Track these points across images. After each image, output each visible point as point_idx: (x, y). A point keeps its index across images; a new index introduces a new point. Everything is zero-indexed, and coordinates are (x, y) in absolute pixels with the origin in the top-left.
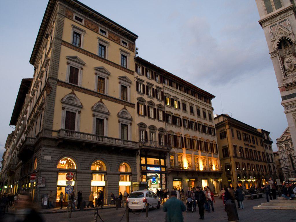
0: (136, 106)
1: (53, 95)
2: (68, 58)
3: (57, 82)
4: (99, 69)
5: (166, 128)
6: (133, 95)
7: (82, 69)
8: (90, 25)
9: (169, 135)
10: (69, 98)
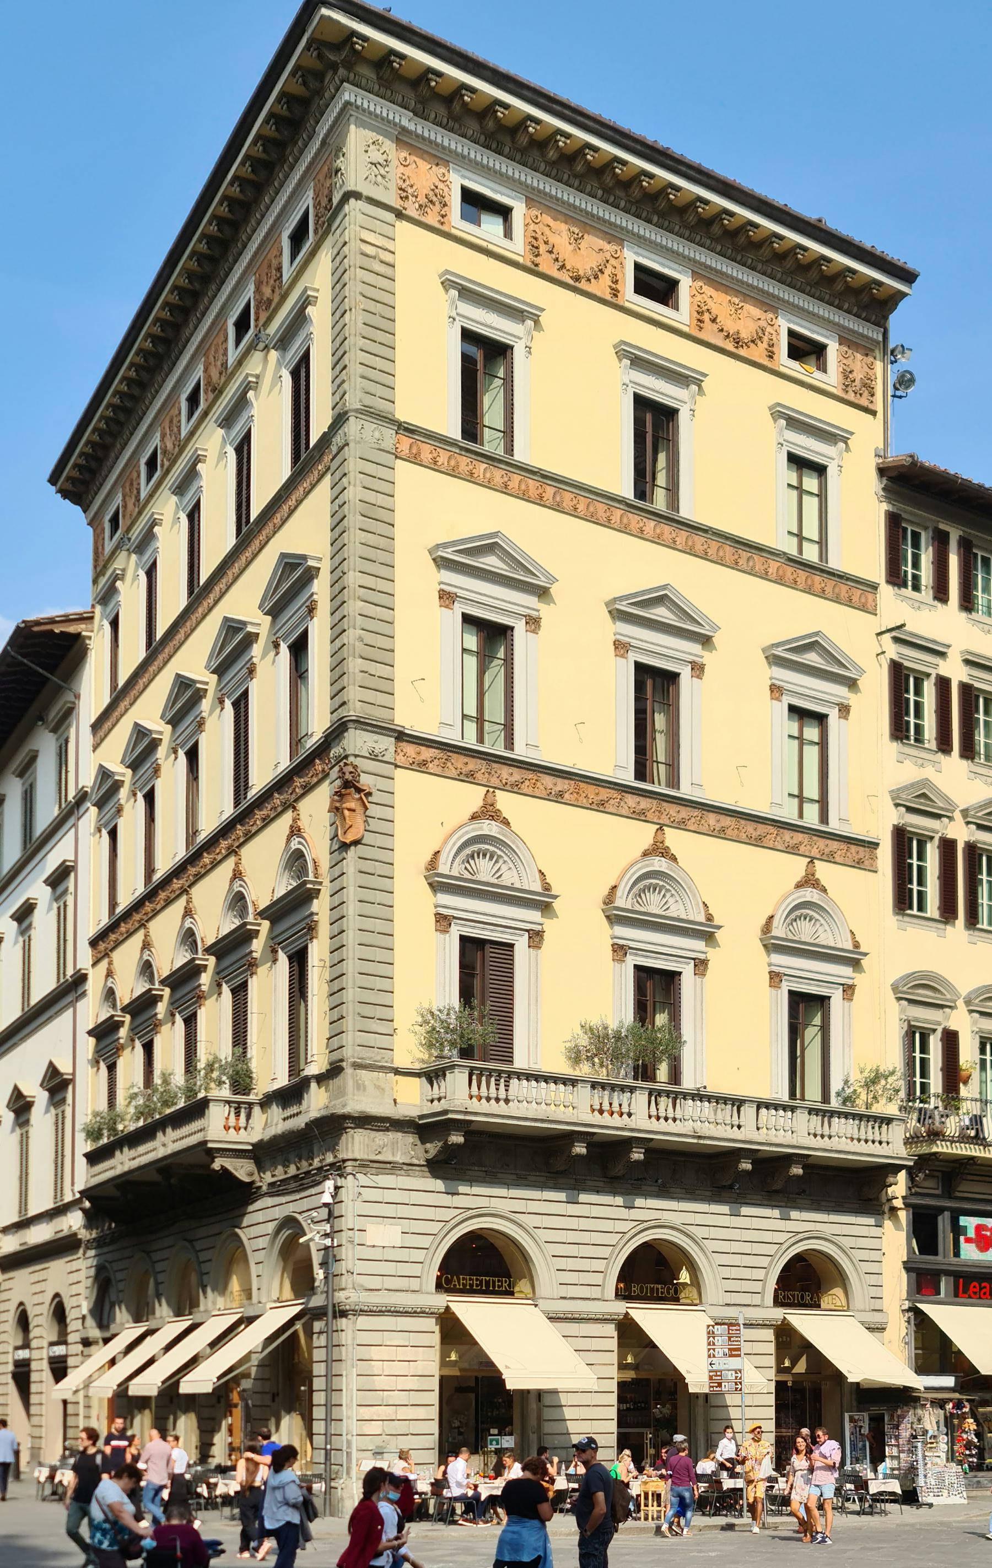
0: (885, 856)
3: (392, 749)
4: (635, 610)
6: (872, 775)
10: (468, 851)
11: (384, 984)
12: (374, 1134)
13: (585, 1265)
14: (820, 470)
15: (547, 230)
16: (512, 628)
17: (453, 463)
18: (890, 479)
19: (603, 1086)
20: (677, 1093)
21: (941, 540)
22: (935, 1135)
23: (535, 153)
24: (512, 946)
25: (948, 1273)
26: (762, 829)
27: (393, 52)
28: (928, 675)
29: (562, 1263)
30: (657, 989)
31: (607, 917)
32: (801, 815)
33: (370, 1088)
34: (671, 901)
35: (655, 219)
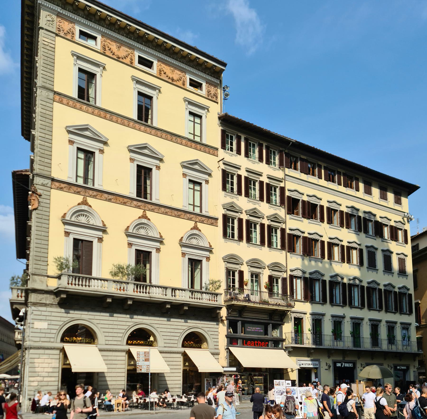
0: (220, 222)
1: (44, 209)
3: (50, 183)
4: (138, 150)
5: (287, 264)
6: (215, 199)
7: (102, 151)
9: (292, 277)
11: (45, 251)
12: (39, 295)
13: (116, 335)
14: (200, 117)
15: (109, 44)
16: (95, 152)
17: (74, 105)
18: (222, 120)
19: (118, 282)
20: (193, 291)
21: (261, 147)
22: (237, 299)
23: (103, 22)
24: (92, 242)
25: (240, 338)
26: (180, 213)
27: (156, 38)
28: (257, 181)
29: (165, 337)
30: (143, 257)
31: (180, 245)
32: (194, 210)
33: (38, 281)
34: (149, 232)
35: (144, 43)
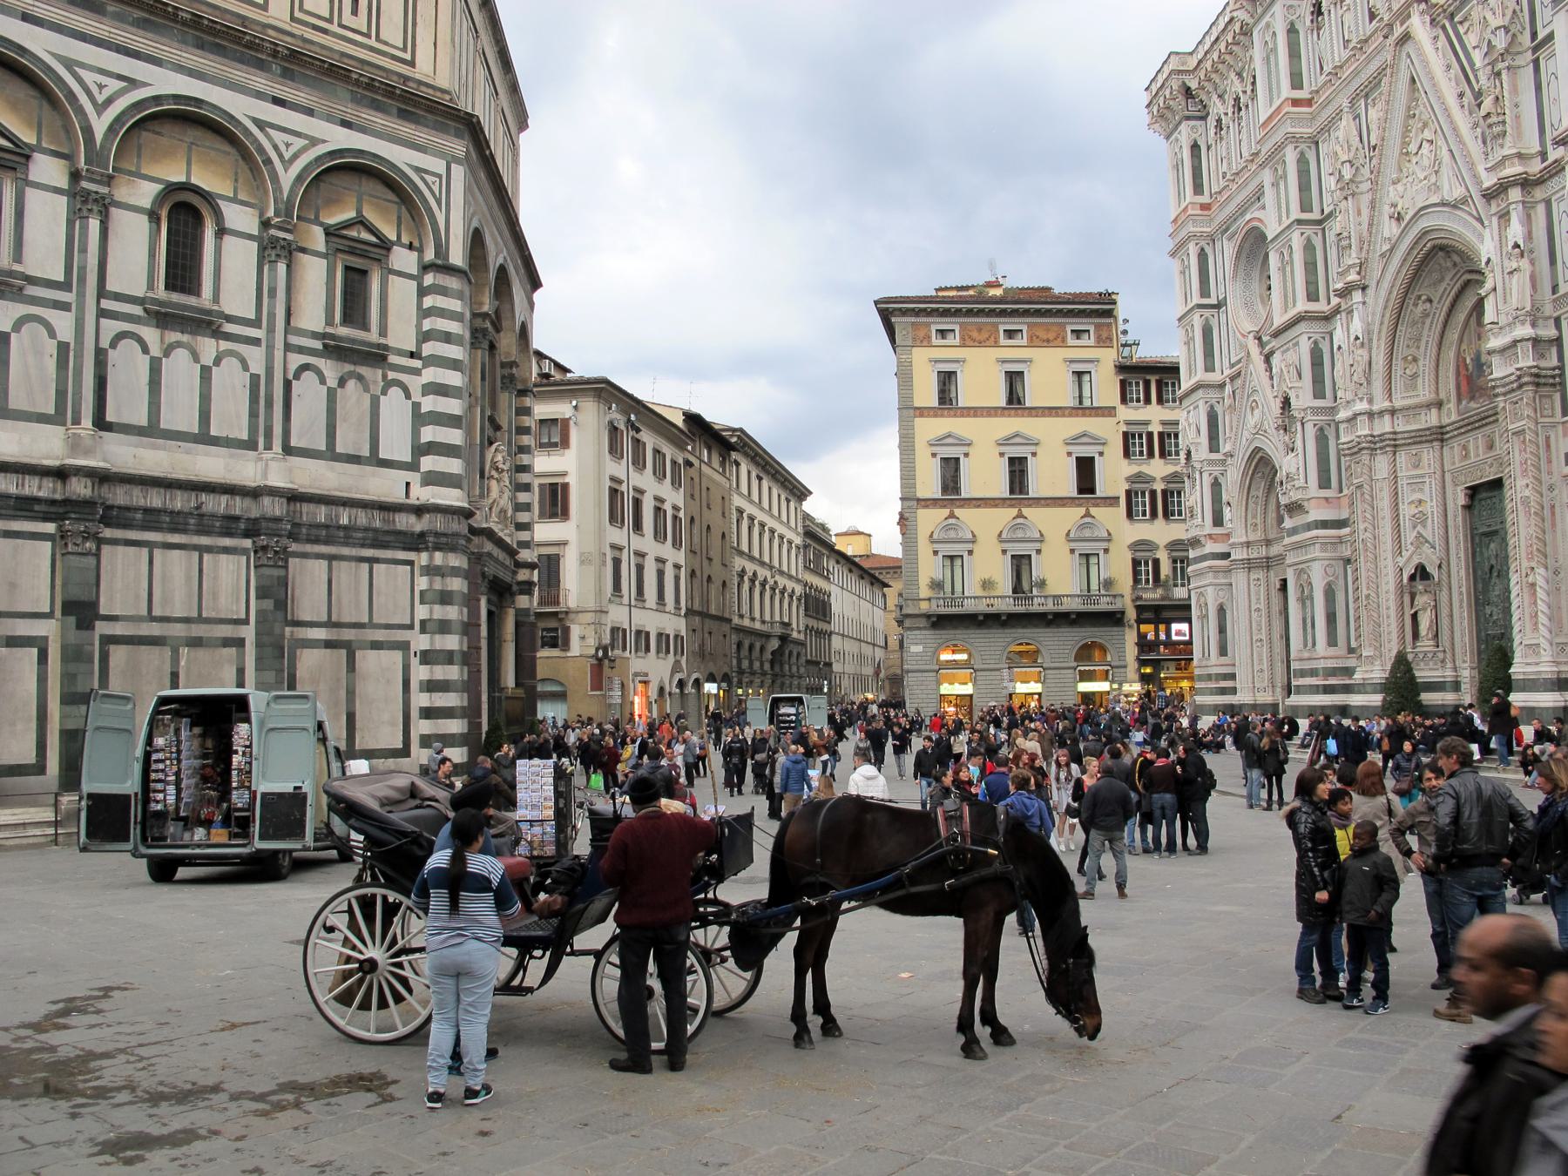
0: (1123, 501)
2: (940, 441)
7: (1034, 454)
8: (975, 334)
